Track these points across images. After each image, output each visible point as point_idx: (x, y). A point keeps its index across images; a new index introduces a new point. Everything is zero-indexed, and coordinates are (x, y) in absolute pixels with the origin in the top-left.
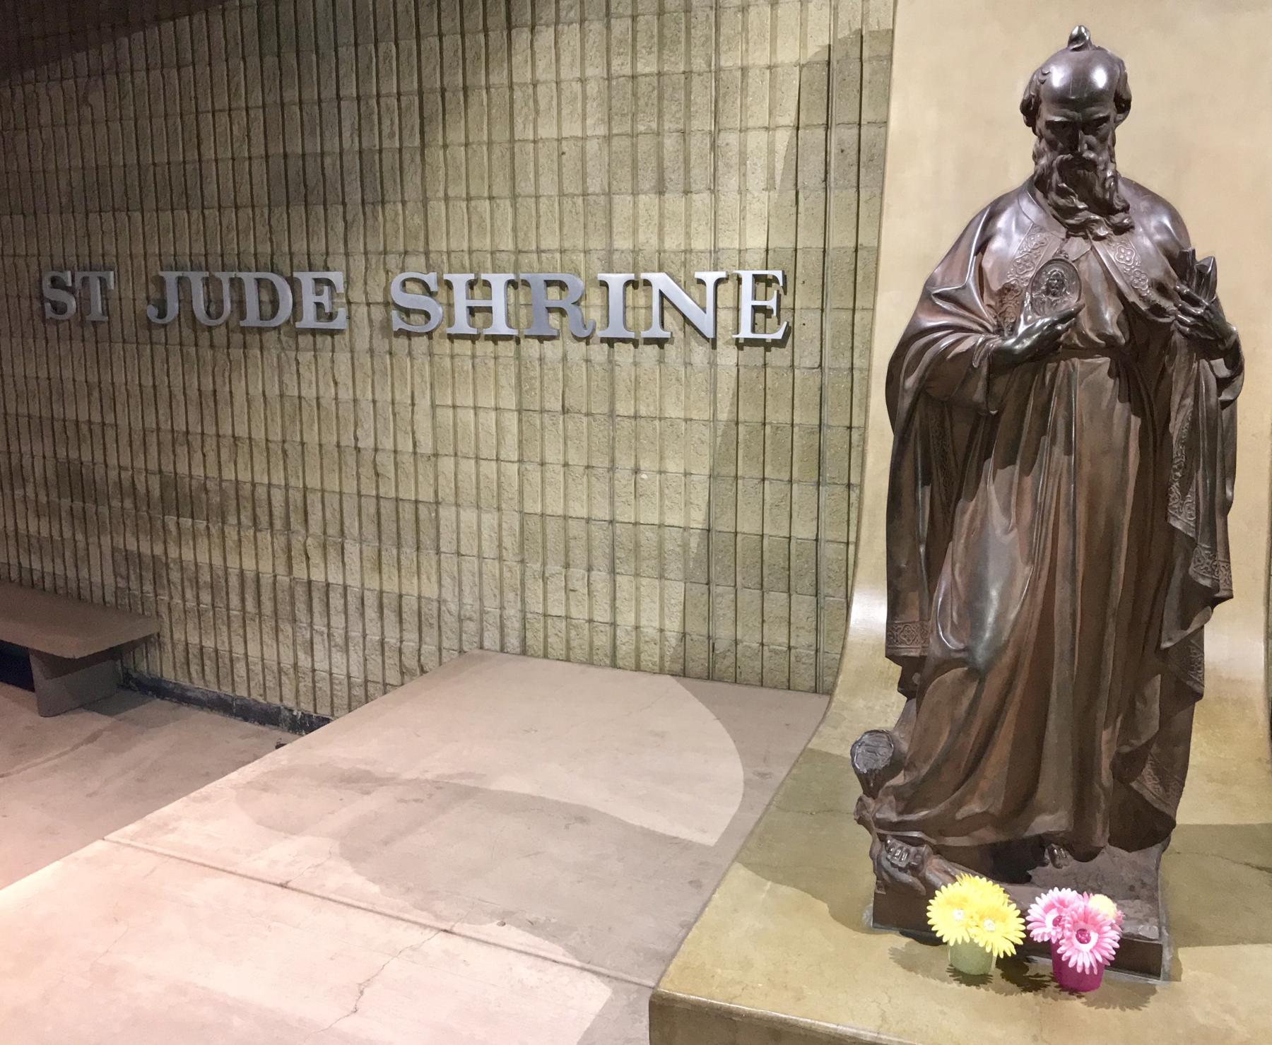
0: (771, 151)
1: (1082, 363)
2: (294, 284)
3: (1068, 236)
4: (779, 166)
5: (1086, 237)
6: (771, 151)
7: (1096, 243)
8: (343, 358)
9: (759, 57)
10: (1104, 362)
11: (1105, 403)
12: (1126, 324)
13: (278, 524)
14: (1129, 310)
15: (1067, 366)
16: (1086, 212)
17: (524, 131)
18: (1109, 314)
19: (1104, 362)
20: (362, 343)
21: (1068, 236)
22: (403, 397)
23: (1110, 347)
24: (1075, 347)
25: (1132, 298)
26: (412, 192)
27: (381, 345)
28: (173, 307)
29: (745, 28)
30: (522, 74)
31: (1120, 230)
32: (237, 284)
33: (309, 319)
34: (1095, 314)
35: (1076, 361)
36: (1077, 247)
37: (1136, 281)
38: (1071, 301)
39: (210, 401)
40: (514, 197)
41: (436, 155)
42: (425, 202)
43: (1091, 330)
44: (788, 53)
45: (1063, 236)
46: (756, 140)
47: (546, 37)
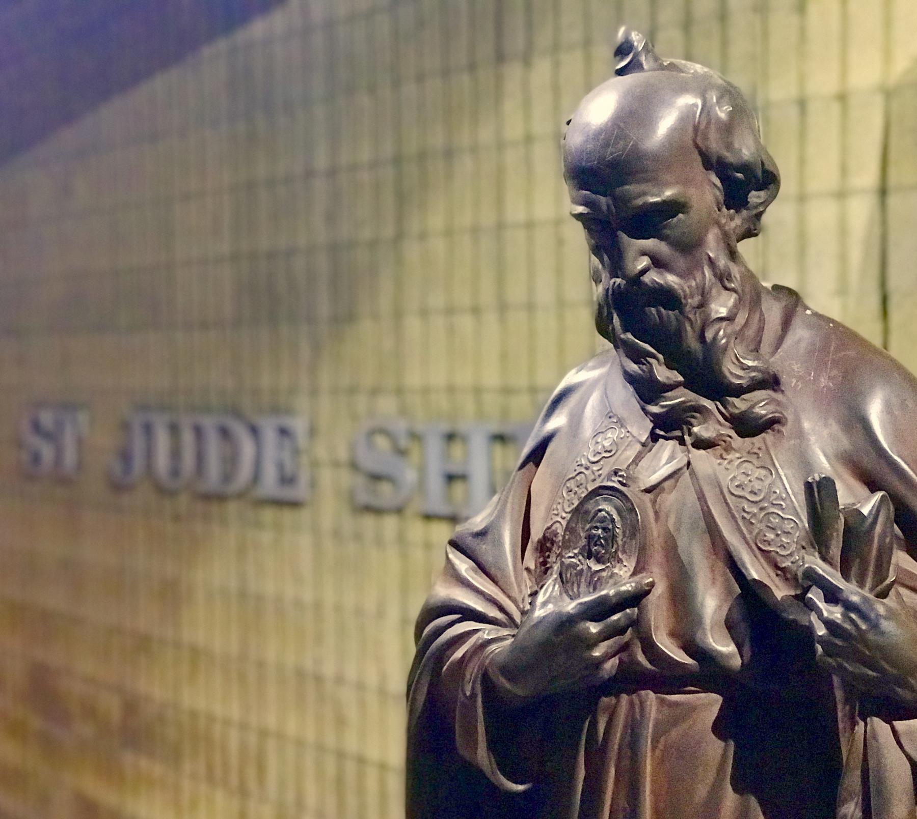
0: (843, 231)
1: (662, 701)
2: (255, 431)
3: (654, 438)
4: (856, 255)
5: (682, 442)
6: (843, 231)
7: (698, 455)
8: (305, 541)
9: (823, 82)
10: (709, 704)
11: (702, 792)
12: (743, 628)
13: (234, 780)
14: (750, 603)
15: (631, 704)
16: (682, 390)
17: (515, 212)
18: (712, 602)
19: (709, 704)
20: (327, 522)
21: (654, 438)
22: (370, 605)
23: (708, 672)
24: (644, 673)
25: (755, 571)
26: (385, 303)
27: (348, 523)
28: (138, 463)
29: (803, 35)
30: (514, 129)
31: (747, 426)
32: (198, 431)
33: (269, 484)
34: (682, 598)
35: (650, 697)
36: (667, 457)
37: (771, 536)
38: (622, 579)
39: (172, 595)
40: (503, 307)
41: (412, 251)
42: (398, 315)
43: (673, 634)
44: (866, 73)
45: (644, 437)
46: (821, 214)
47: (542, 69)
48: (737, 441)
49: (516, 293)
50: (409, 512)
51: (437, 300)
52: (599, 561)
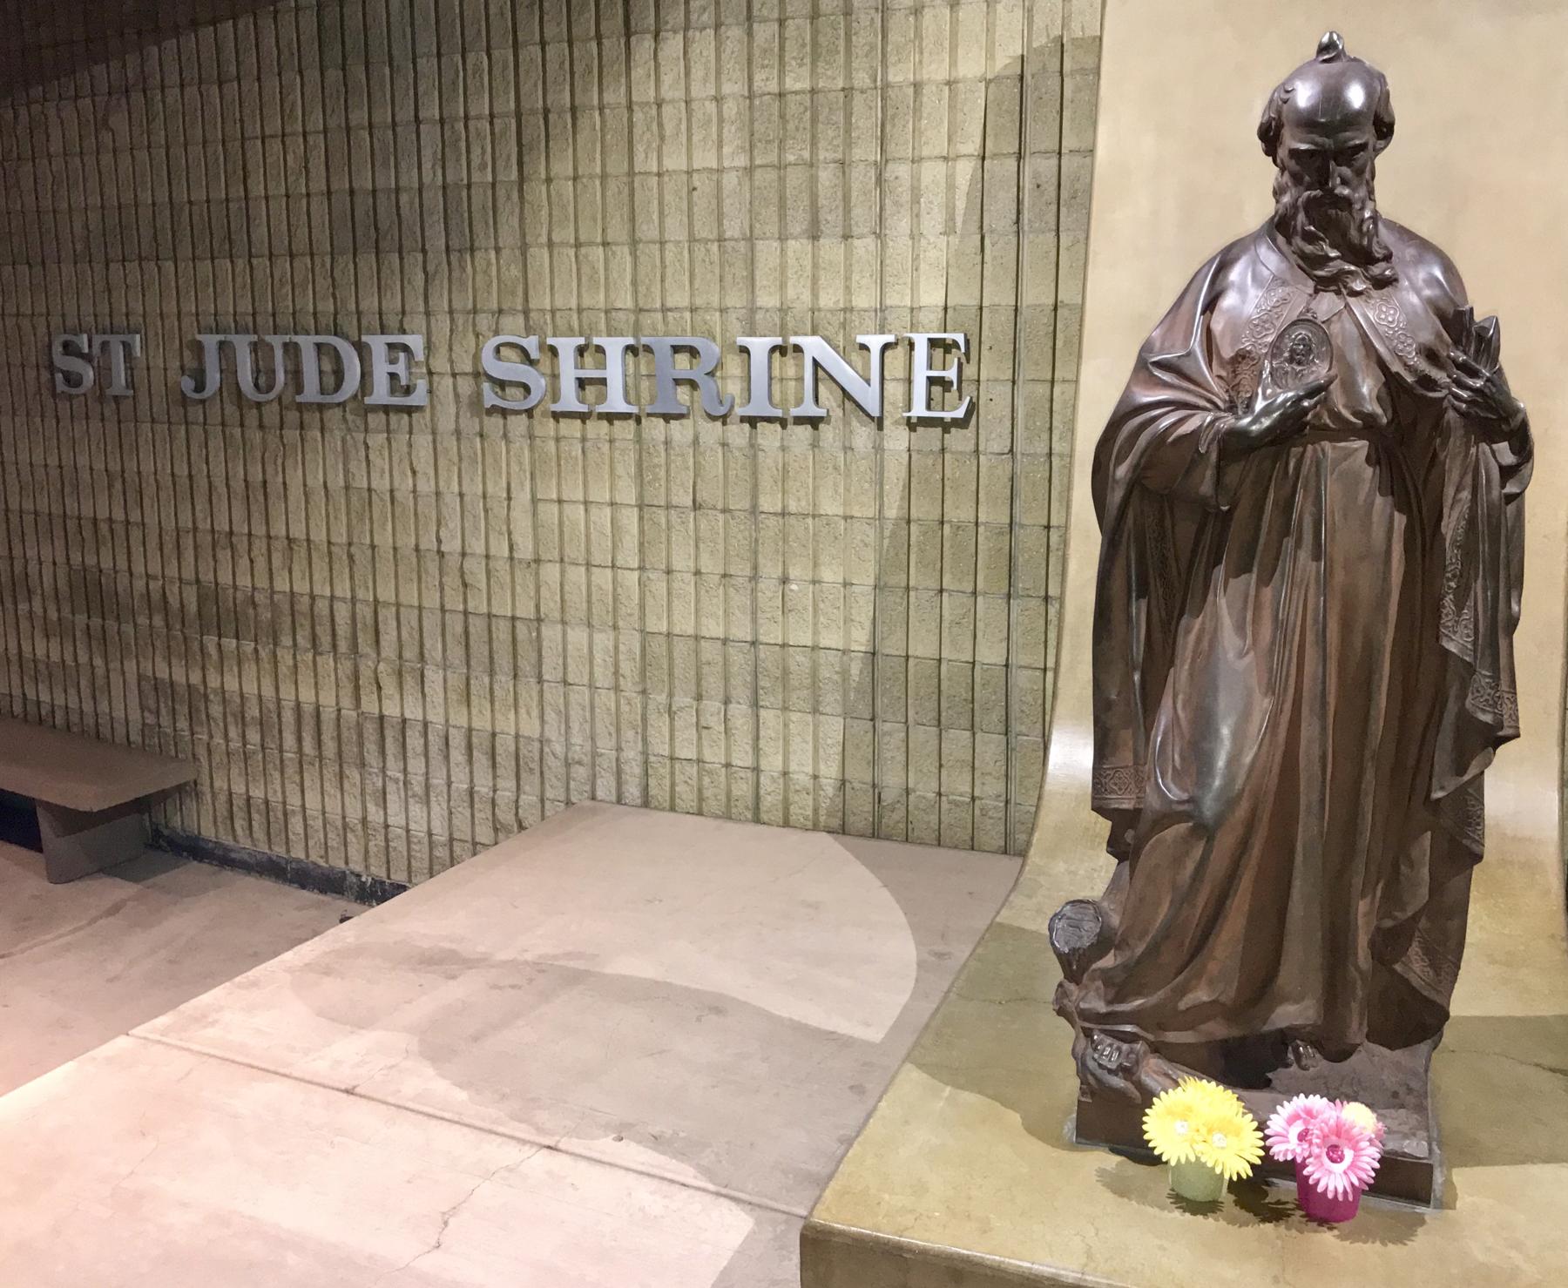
0: (951, 186)
1: (1334, 448)
2: (362, 350)
3: (1316, 291)
4: (961, 204)
5: (1338, 293)
6: (951, 186)
7: (1351, 300)
8: (423, 441)
9: (936, 70)
10: (1361, 446)
11: (1362, 497)
12: (1387, 400)
13: (343, 646)
15: (1315, 451)
16: (1339, 262)
17: (646, 161)
18: (1368, 387)
19: (1361, 446)
20: (446, 423)
21: (1316, 291)
23: (1369, 427)
24: (1326, 427)
25: (1396, 367)
26: (508, 237)
27: (470, 425)
28: (213, 378)
29: (918, 35)
30: (644, 92)
31: (1381, 283)
32: (292, 350)
33: (381, 393)
35: (1327, 445)
38: (1320, 371)
39: (259, 495)
40: (634, 243)
41: (537, 191)
42: (524, 248)
44: (972, 66)
45: (1311, 291)
46: (932, 173)
47: (673, 45)
48: (1374, 293)
49: (647, 230)
50: (537, 413)
51: (564, 234)
52: (1299, 363)
